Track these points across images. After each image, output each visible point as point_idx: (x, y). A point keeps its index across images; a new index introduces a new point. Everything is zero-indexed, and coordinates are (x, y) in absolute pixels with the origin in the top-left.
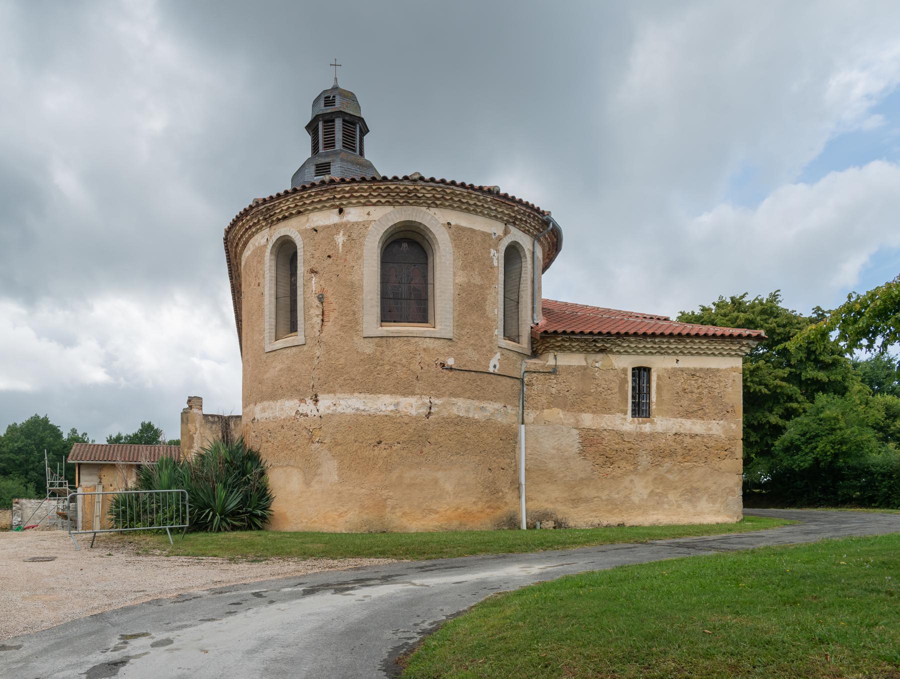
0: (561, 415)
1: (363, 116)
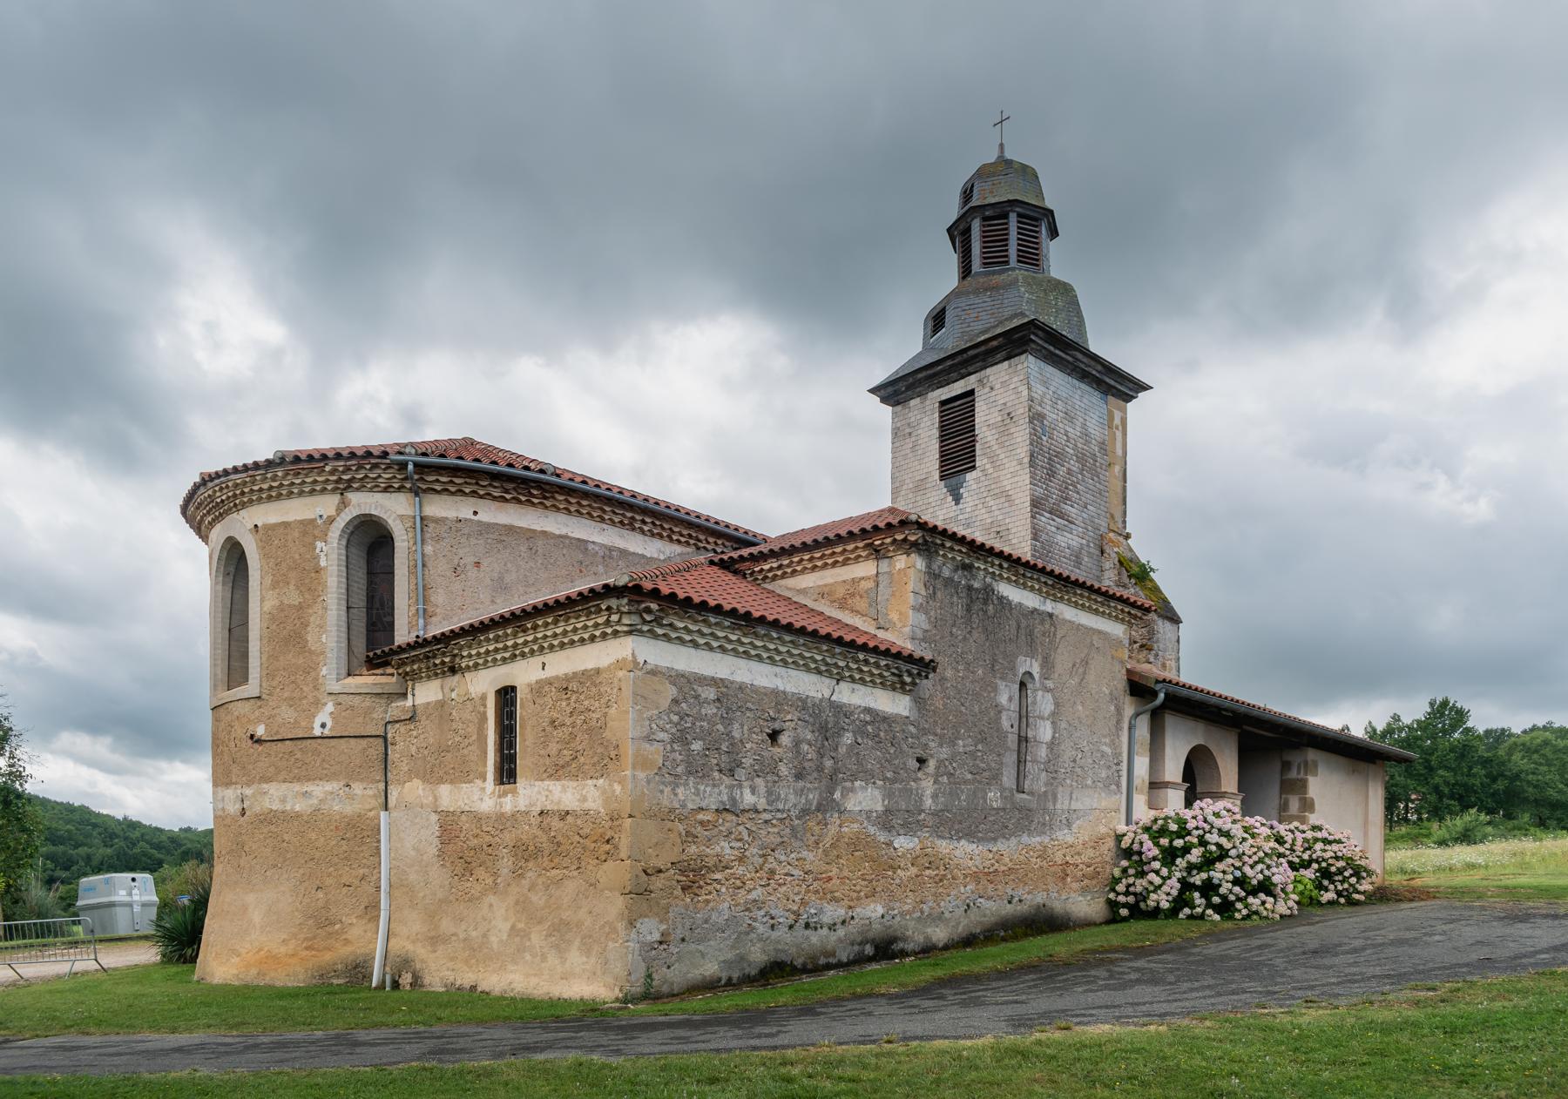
0: (420, 792)
1: (1049, 204)
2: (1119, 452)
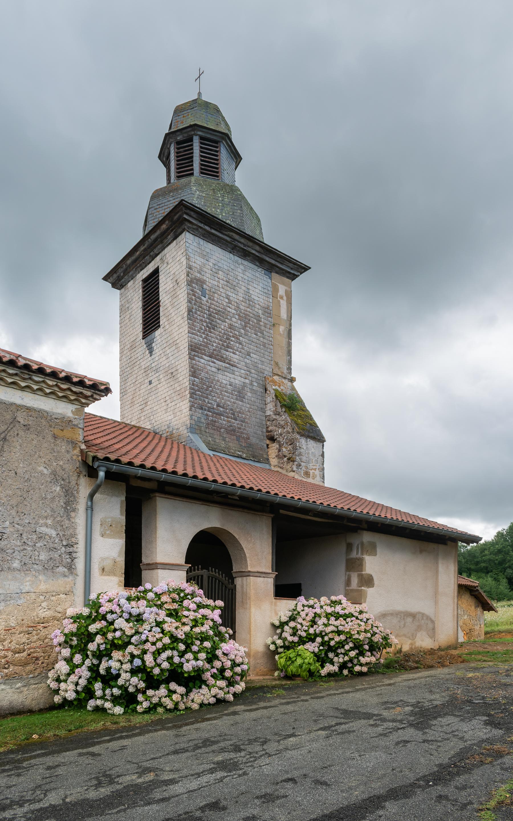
2: (284, 315)
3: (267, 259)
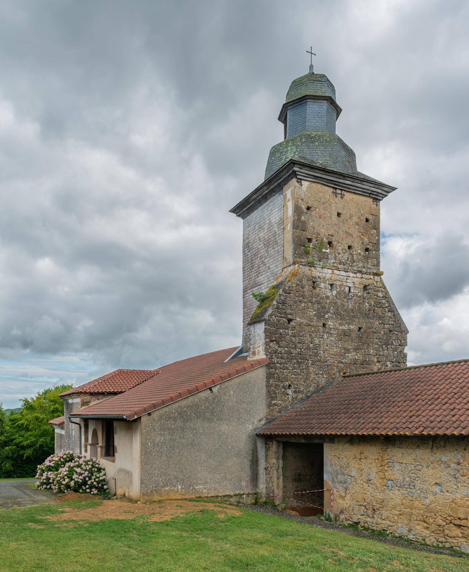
3: (272, 187)
